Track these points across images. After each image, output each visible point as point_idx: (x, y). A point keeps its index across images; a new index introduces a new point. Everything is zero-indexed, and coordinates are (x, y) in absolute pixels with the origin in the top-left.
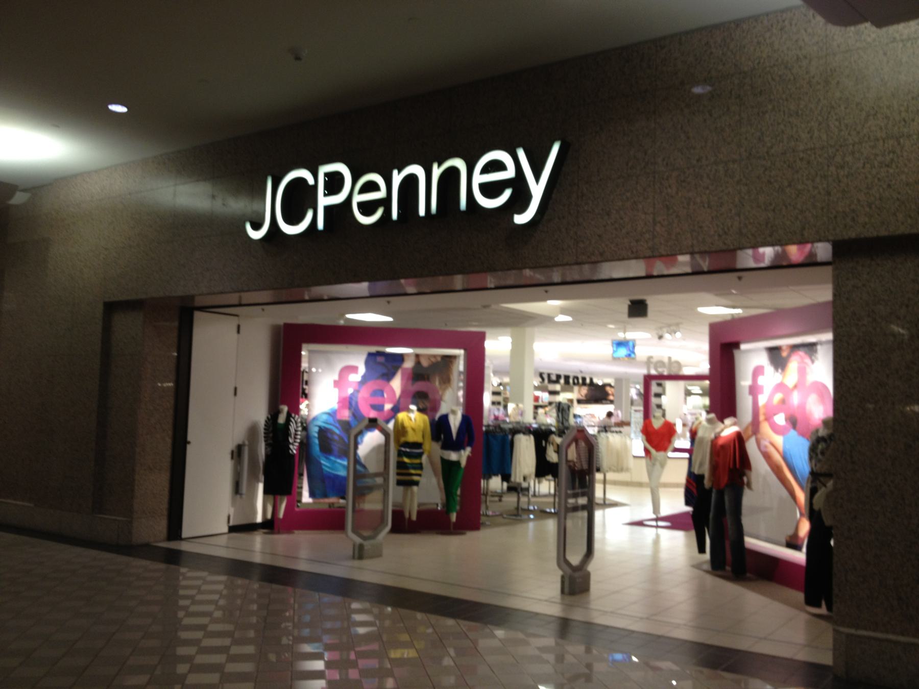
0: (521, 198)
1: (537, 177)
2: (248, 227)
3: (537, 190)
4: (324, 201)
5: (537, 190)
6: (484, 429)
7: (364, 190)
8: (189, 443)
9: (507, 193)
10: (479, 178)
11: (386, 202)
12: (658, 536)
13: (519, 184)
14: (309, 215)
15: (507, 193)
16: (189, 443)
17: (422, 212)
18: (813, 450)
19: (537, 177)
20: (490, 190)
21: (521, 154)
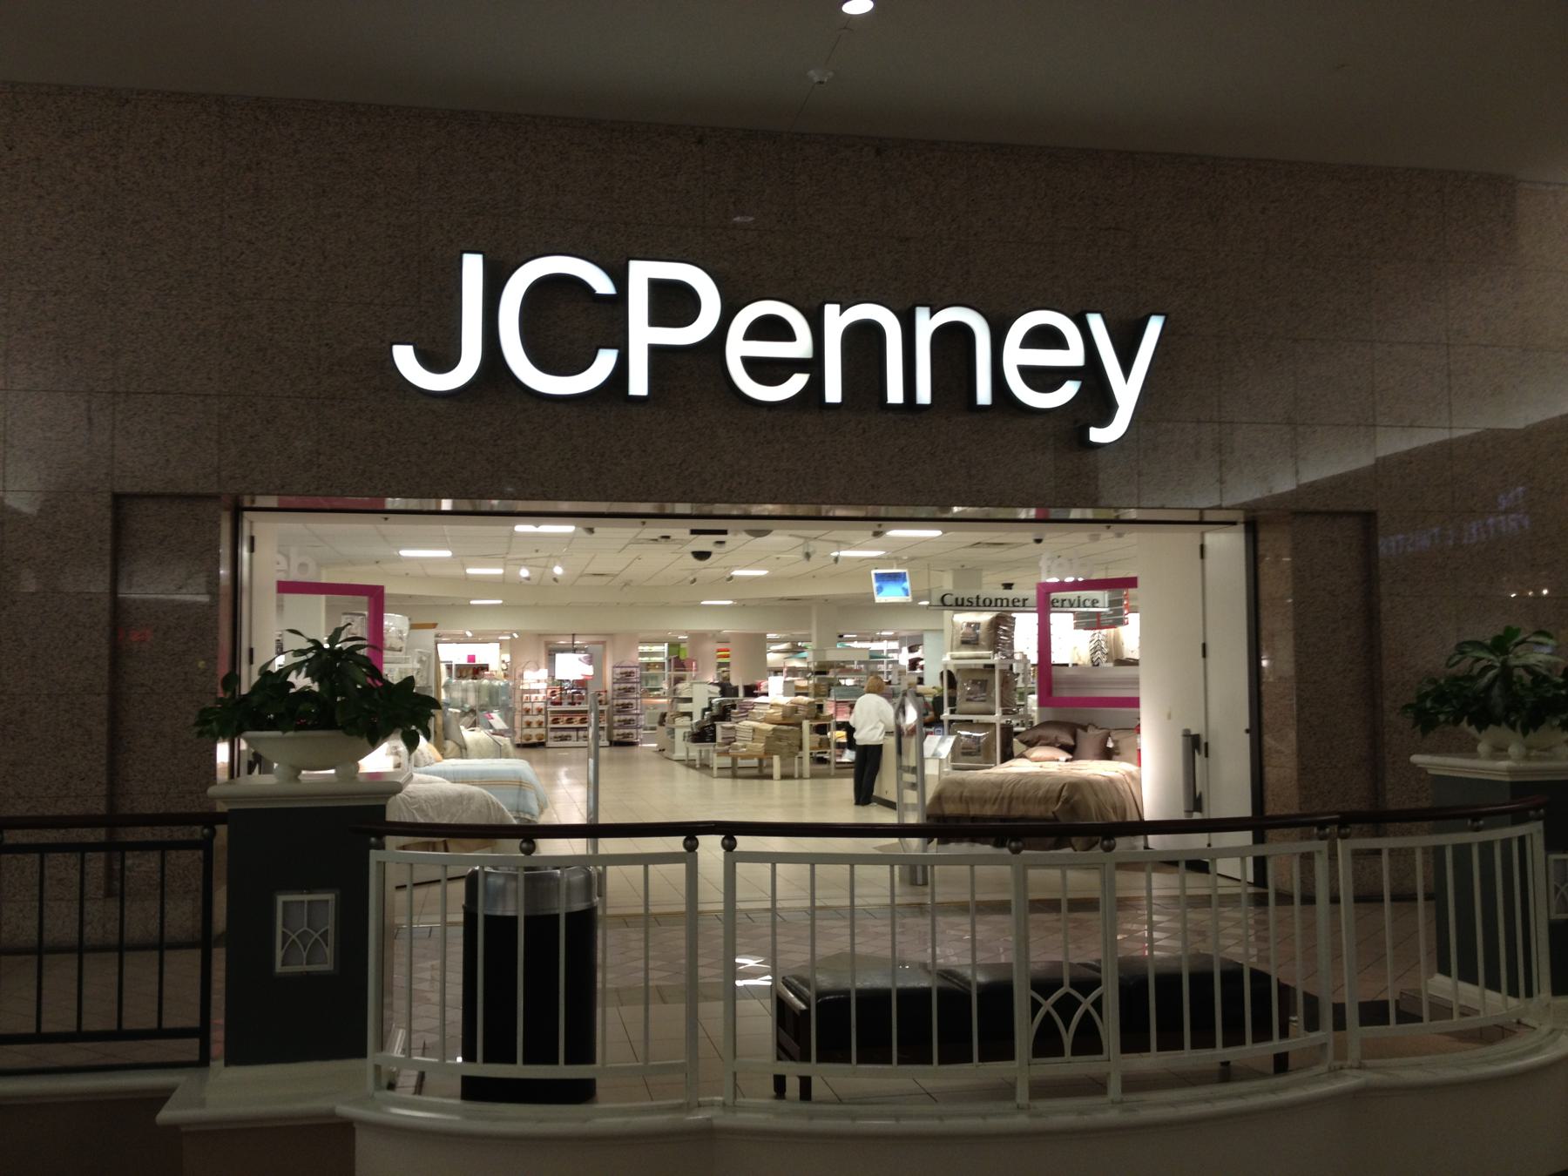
0: (1097, 401)
1: (1126, 366)
2: (405, 358)
3: (1127, 391)
4: (643, 334)
5: (1127, 391)
6: (414, 691)
7: (761, 329)
8: (1247, 731)
9: (1070, 390)
10: (1015, 356)
11: (814, 365)
12: (1139, 502)
13: (1092, 372)
14: (606, 361)
15: (1070, 390)
16: (1247, 731)
17: (895, 395)
18: (398, 783)
19: (1126, 366)
20: (1042, 379)
21: (1096, 322)
